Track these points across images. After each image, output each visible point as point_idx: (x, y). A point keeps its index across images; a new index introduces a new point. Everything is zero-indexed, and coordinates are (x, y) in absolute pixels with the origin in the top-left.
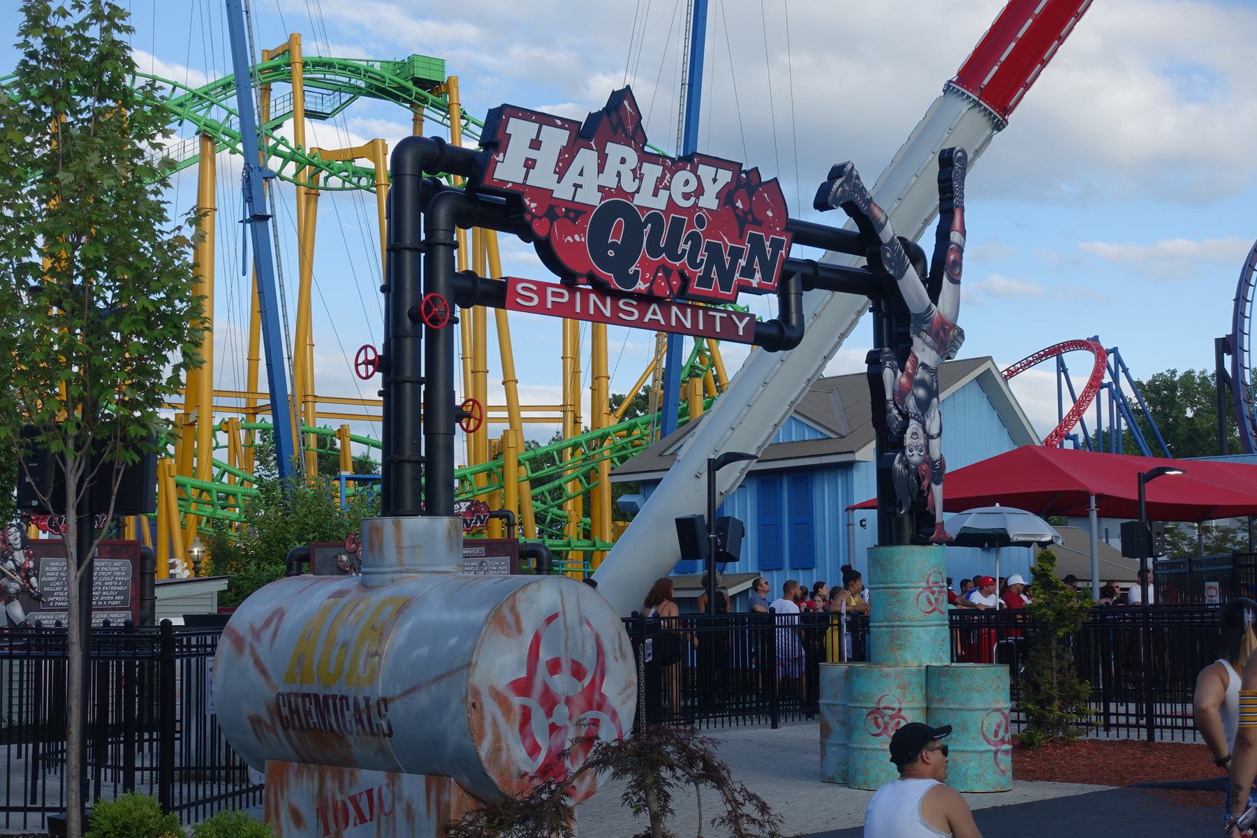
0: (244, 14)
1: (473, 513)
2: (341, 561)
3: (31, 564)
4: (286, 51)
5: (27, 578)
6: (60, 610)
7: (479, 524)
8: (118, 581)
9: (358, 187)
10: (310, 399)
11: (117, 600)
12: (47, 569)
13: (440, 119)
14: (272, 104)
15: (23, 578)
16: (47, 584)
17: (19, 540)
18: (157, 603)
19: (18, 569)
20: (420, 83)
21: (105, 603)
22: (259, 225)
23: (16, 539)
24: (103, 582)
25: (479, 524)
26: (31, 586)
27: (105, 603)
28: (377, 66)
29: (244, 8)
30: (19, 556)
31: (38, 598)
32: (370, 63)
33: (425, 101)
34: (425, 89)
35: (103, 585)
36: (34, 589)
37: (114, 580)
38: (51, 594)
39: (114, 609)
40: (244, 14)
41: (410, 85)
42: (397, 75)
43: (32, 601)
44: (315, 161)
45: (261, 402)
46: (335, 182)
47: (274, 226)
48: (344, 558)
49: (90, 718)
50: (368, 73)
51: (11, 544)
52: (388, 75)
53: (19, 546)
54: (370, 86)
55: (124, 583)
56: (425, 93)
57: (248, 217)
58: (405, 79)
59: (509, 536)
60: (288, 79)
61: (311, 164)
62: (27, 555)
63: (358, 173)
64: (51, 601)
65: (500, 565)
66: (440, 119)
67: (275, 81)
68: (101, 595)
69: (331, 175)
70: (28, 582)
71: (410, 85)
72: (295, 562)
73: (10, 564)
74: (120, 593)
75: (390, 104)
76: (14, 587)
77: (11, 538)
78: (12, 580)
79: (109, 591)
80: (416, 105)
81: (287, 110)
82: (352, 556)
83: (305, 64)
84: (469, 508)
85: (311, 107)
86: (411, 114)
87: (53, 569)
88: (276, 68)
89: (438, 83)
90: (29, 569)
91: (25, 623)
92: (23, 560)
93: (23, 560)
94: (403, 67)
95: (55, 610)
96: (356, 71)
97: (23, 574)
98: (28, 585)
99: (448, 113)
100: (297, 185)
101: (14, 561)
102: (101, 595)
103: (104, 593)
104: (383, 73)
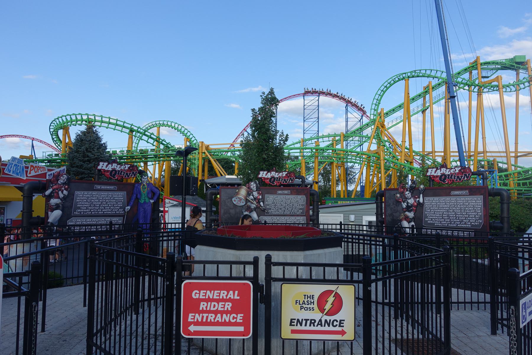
0: (446, 40)
1: (463, 173)
2: (397, 197)
3: (261, 197)
4: (476, 61)
5: (259, 202)
6: (274, 216)
7: (466, 179)
8: (300, 204)
9: (494, 91)
10: (485, 152)
11: (299, 212)
12: (268, 199)
13: (525, 72)
14: (473, 76)
15: (257, 203)
16: (268, 205)
17: (255, 187)
18: (375, 211)
19: (255, 199)
20: (517, 63)
21: (294, 213)
22: (452, 99)
23: (254, 187)
24: (293, 205)
25: (466, 179)
26: (260, 206)
27: (294, 213)
28: (504, 61)
29: (446, 38)
30: (255, 194)
31: (264, 210)
32: (502, 61)
33: (520, 68)
34: (520, 65)
35: (293, 205)
36: (262, 207)
37: (298, 204)
38: (270, 209)
39: (298, 216)
40: (446, 40)
41: (514, 64)
42: (510, 62)
43: (262, 212)
44: (479, 85)
45: (472, 154)
46: (485, 90)
47: (457, 99)
48: (398, 195)
49: (41, 303)
50: (501, 63)
51: (252, 189)
52: (507, 63)
53: (255, 190)
54: (502, 67)
55: (302, 205)
56: (520, 66)
57: (449, 97)
58: (513, 63)
59: (483, 185)
60: (477, 69)
61: (478, 86)
62: (258, 193)
63: (494, 87)
64: (270, 212)
65: (477, 200)
66: (525, 72)
67: (473, 70)
68: (292, 210)
69: (484, 88)
70: (259, 204)
71: (514, 64)
72: (379, 197)
73: (251, 197)
74: (301, 209)
75: (510, 71)
76: (253, 206)
77: (252, 187)
78: (252, 203)
79: (296, 208)
80: (516, 70)
81: (477, 77)
82: (402, 195)
83: (481, 64)
84: (460, 170)
85: (484, 75)
86: (515, 73)
87: (270, 199)
88: (473, 67)
89: (524, 62)
90: (260, 199)
91: (258, 221)
92: (257, 195)
93: (257, 195)
94: (512, 60)
95: (272, 216)
96: (497, 63)
97: (257, 201)
98: (259, 205)
99: (527, 70)
100: (469, 91)
101: (253, 195)
102: (292, 210)
103: (293, 209)
104: (506, 62)
